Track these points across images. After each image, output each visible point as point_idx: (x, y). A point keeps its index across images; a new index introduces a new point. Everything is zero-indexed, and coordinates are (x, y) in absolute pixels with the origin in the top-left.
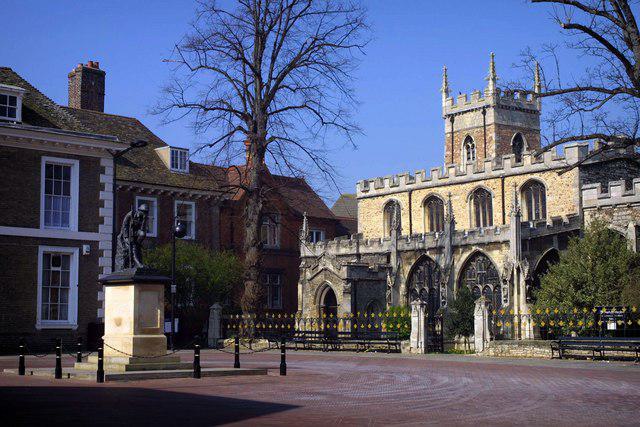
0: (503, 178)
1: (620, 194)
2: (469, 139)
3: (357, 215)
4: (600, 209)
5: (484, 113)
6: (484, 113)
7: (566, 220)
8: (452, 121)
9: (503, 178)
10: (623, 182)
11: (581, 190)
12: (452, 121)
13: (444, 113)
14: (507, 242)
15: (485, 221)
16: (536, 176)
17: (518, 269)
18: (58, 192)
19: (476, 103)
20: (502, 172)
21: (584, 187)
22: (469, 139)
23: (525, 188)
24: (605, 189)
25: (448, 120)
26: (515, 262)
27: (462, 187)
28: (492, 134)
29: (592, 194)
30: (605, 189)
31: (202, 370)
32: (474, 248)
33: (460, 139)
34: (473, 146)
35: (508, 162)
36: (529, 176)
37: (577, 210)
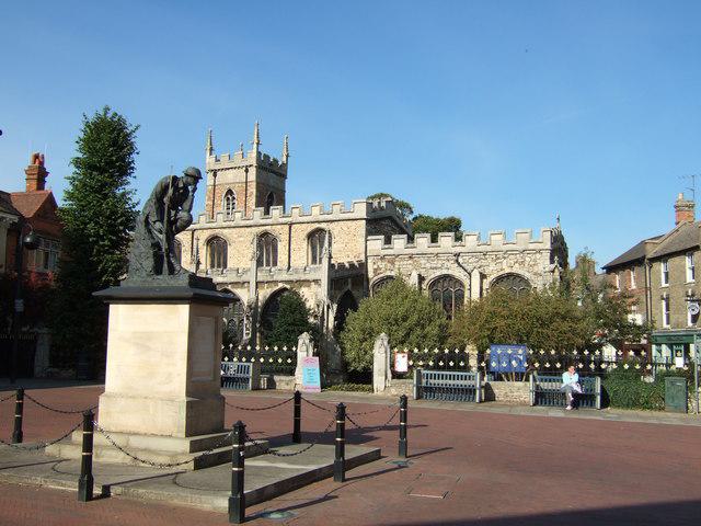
0: (291, 225)
1: (451, 244)
2: (230, 192)
3: (8, 239)
4: (383, 258)
5: (247, 171)
6: (247, 171)
7: (347, 265)
8: (215, 175)
9: (291, 225)
10: (428, 235)
11: (366, 241)
12: (215, 175)
13: (208, 168)
14: (316, 281)
15: (268, 261)
16: (323, 226)
17: (328, 307)
18: (219, 266)
19: (238, 161)
20: (290, 219)
21: (369, 238)
22: (230, 192)
23: (311, 236)
24: (388, 241)
25: (211, 174)
26: (327, 301)
27: (249, 229)
28: (253, 189)
29: (376, 244)
30: (388, 241)
31: (35, 177)
32: (280, 285)
33: (221, 192)
34: (234, 198)
35: (220, 216)
36: (317, 225)
37: (363, 258)
